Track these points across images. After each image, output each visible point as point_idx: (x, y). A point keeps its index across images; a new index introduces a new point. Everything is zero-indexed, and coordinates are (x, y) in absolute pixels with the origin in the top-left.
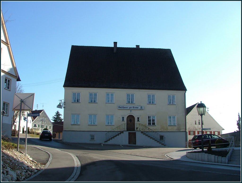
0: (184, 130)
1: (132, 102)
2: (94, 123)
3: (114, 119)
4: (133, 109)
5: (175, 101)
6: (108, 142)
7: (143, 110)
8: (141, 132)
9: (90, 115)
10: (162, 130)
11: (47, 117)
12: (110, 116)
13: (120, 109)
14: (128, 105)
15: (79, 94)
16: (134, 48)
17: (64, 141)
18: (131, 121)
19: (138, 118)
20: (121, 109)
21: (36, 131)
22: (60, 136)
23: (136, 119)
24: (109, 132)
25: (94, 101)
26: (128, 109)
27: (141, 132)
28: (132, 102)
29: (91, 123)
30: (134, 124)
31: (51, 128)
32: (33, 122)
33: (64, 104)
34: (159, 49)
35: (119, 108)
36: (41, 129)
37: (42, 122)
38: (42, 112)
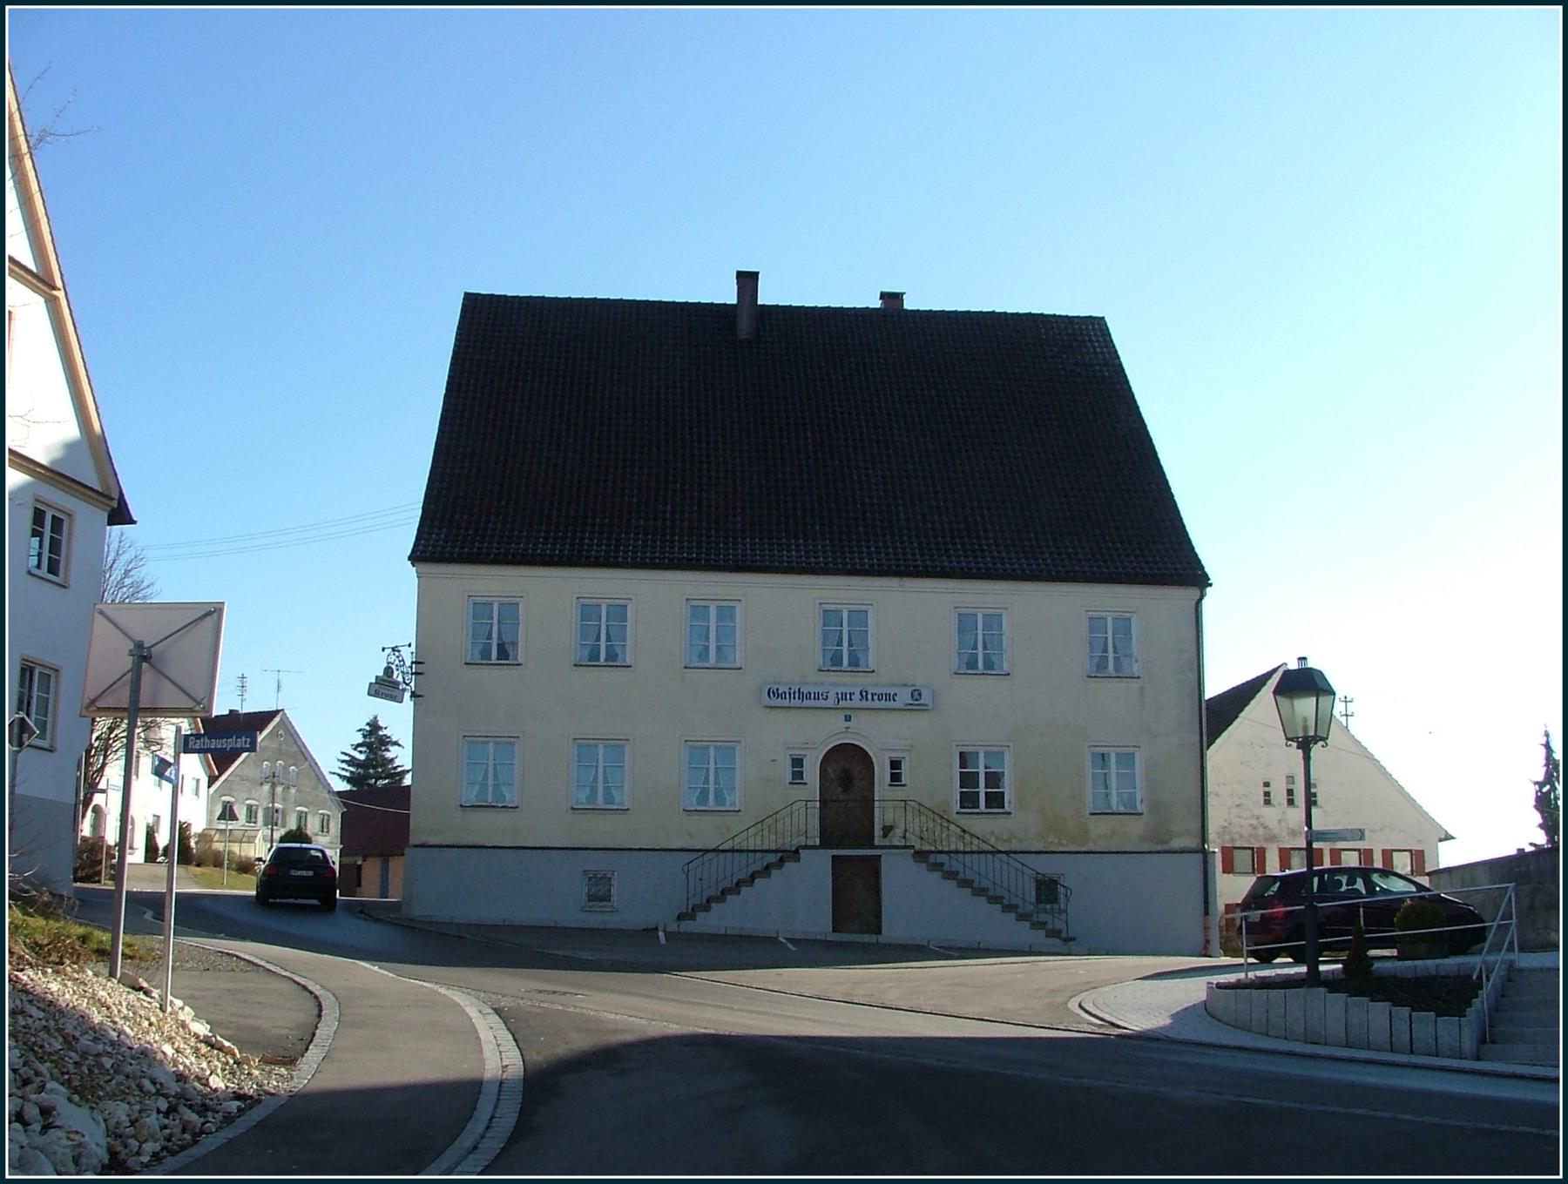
0: (1193, 843)
1: (854, 661)
2: (609, 797)
4: (864, 704)
6: (700, 915)
7: (923, 709)
9: (585, 747)
10: (1052, 842)
11: (301, 754)
13: (779, 702)
15: (510, 610)
17: (417, 911)
18: (846, 780)
19: (895, 764)
20: (786, 703)
21: (235, 848)
23: (882, 772)
24: (707, 851)
25: (612, 655)
26: (831, 702)
28: (854, 661)
30: (868, 802)
31: (332, 830)
32: (212, 790)
36: (262, 832)
37: (274, 786)
38: (270, 727)
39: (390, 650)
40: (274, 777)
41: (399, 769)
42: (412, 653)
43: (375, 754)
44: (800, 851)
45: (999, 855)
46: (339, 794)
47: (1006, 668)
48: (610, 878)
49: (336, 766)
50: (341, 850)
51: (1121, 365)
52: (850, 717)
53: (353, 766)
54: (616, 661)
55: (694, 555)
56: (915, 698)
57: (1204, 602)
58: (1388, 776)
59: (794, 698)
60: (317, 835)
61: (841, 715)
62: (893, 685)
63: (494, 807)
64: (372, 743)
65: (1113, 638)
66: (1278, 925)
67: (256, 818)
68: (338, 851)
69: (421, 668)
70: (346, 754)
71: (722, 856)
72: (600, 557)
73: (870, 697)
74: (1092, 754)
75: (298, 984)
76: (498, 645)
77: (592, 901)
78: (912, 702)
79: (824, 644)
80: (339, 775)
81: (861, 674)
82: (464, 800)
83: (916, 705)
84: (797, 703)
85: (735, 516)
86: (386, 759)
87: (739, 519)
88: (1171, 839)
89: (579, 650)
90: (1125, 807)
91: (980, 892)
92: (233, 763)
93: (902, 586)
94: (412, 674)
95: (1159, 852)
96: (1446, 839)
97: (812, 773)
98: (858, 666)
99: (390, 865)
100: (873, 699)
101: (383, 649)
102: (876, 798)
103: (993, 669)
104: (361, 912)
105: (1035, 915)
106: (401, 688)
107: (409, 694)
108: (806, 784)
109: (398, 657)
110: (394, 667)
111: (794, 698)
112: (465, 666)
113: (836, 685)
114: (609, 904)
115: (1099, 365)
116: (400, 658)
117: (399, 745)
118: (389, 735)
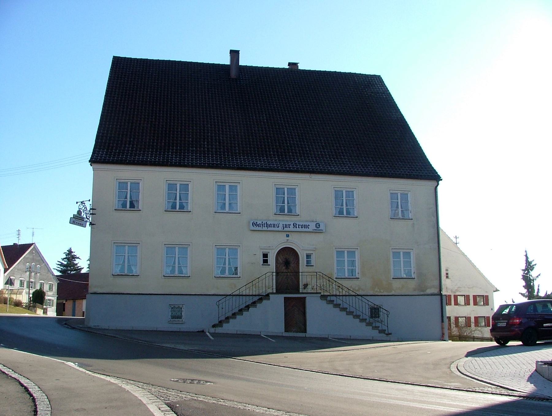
0: (436, 291)
1: (290, 211)
2: (181, 271)
3: (239, 260)
4: (295, 229)
5: (410, 209)
6: (225, 325)
7: (321, 232)
8: (321, 296)
9: (170, 248)
10: (377, 291)
11: (42, 260)
12: (229, 249)
13: (258, 228)
14: (280, 218)
15: (136, 186)
16: (283, 70)
17: (92, 324)
18: (287, 263)
19: (308, 256)
20: (260, 229)
21: (14, 297)
22: (76, 309)
23: (303, 260)
24: (227, 295)
25: (182, 207)
26: (280, 229)
27: (321, 296)
28: (290, 211)
29: (173, 271)
30: (297, 273)
31: (54, 290)
32: (6, 274)
33: (92, 214)
34: (350, 74)
35: (253, 228)
36: (26, 290)
37: (30, 272)
38: (30, 250)
39: (80, 203)
40: (30, 268)
41: (79, 268)
42: (90, 205)
43: (71, 262)
44: (270, 295)
45: (358, 297)
46: (56, 276)
47: (356, 215)
48: (182, 308)
49: (56, 266)
50: (57, 297)
51: (390, 93)
52: (289, 235)
53: (62, 266)
54: (183, 209)
55: (219, 162)
56: (317, 227)
57: (438, 187)
58: (474, 266)
59: (264, 227)
60: (48, 291)
61: (285, 234)
62: (307, 221)
63: (128, 275)
64: (69, 258)
65: (401, 202)
66: (517, 328)
67: (23, 285)
68: (56, 298)
69: (94, 212)
70: (59, 262)
71: (234, 297)
72: (177, 162)
73: (297, 226)
74: (393, 252)
75: (22, 385)
76: (130, 201)
77: (173, 318)
78: (316, 229)
79: (277, 203)
80: (56, 270)
81: (293, 216)
82: (114, 272)
83: (318, 230)
84: (265, 228)
85: (235, 147)
86: (74, 264)
87: (237, 148)
88: (426, 289)
89: (167, 204)
90: (406, 276)
91: (350, 313)
92: (14, 264)
93: (311, 178)
94: (90, 214)
95: (421, 295)
96: (496, 291)
97: (272, 259)
98: (291, 212)
99: (76, 303)
100: (299, 227)
101: (77, 203)
102: (300, 271)
103: (350, 215)
104: (65, 324)
105: (374, 323)
106: (85, 220)
107: (89, 223)
108: (269, 265)
109: (84, 206)
110: (82, 210)
111: (264, 227)
112: (115, 211)
113: (283, 221)
114: (180, 320)
115: (381, 93)
116: (85, 207)
117: (79, 259)
118: (75, 255)
